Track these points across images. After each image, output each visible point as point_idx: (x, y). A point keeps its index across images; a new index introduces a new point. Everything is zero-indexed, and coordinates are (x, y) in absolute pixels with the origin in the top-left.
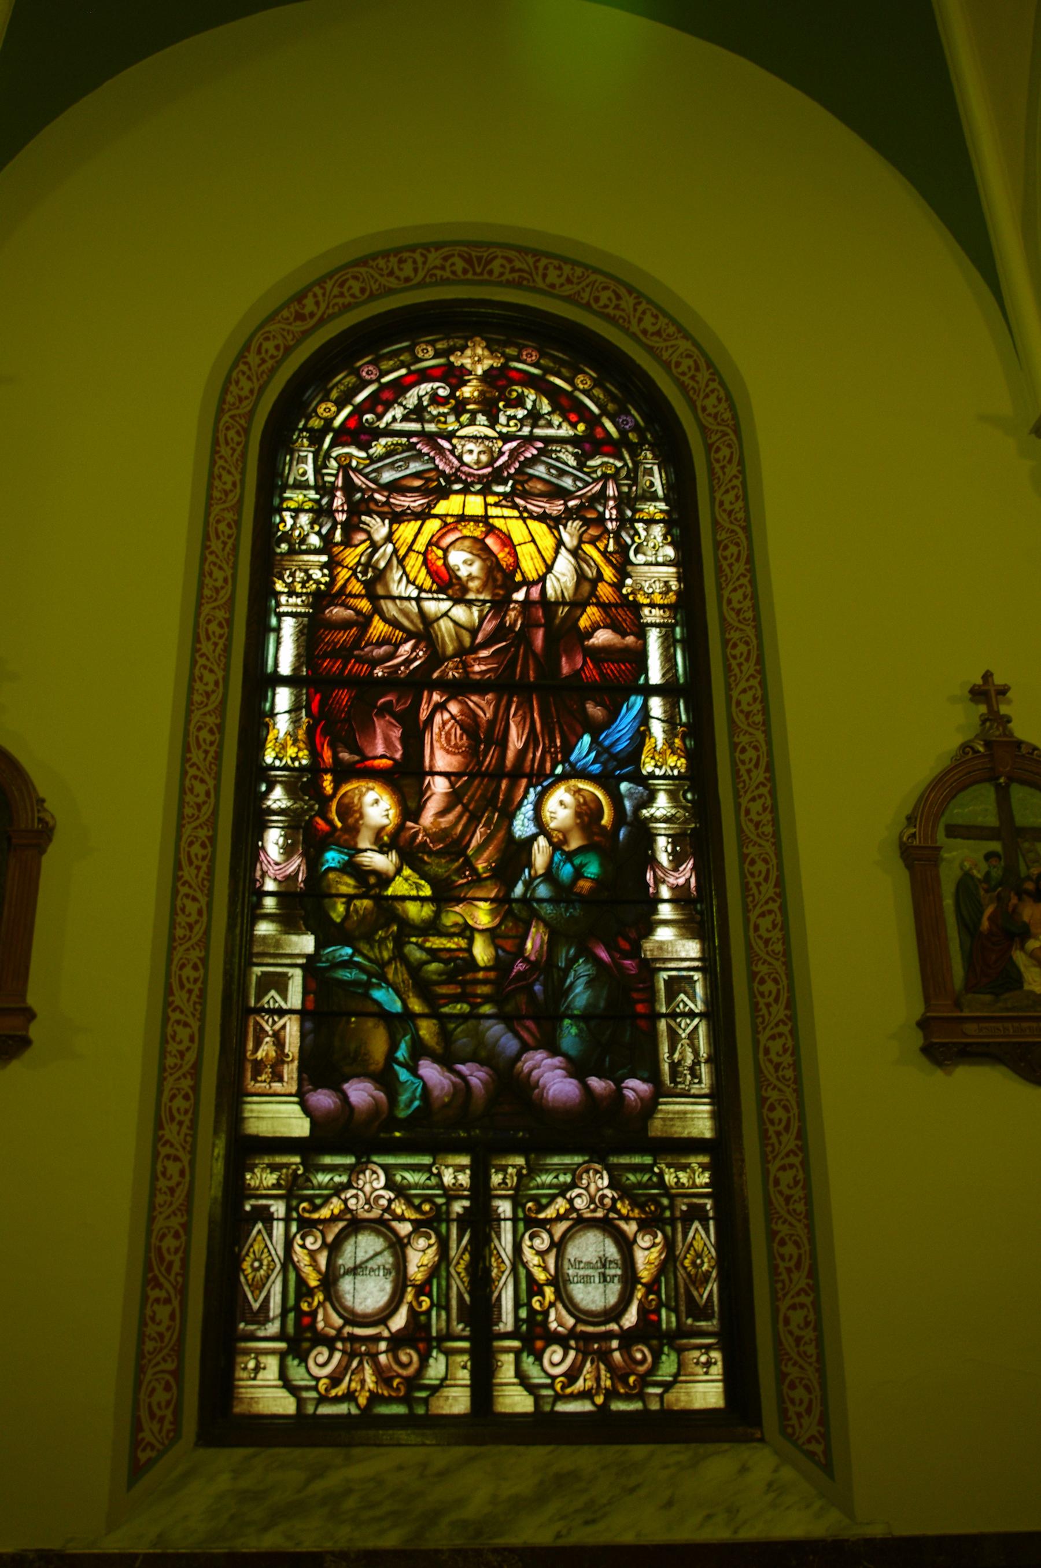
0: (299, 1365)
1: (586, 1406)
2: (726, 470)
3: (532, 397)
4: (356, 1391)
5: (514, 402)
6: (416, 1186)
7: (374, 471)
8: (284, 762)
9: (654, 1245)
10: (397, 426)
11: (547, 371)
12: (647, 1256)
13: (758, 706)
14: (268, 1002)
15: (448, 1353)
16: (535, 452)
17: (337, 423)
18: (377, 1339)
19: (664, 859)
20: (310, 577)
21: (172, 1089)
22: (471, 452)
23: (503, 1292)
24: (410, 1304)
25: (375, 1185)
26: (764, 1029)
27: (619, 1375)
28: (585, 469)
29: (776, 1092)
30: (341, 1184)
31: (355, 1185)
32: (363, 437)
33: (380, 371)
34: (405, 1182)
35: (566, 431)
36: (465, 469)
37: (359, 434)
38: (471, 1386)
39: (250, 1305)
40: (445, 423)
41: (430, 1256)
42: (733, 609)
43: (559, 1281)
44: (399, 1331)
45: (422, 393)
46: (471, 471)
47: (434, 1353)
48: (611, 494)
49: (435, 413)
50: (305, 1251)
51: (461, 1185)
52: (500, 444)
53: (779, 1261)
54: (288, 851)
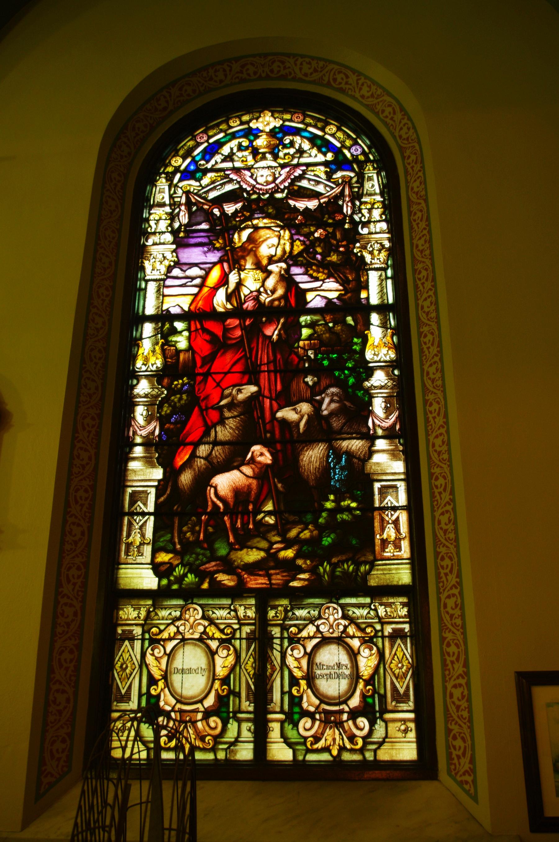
1: (325, 757)
2: (436, 420)
7: (205, 193)
9: (228, 655)
11: (308, 125)
12: (367, 662)
13: (433, 307)
14: (387, 503)
15: (239, 721)
16: (301, 172)
17: (182, 168)
18: (196, 711)
20: (165, 258)
22: (262, 176)
24: (217, 690)
26: (438, 508)
28: (332, 180)
29: (457, 727)
30: (176, 617)
35: (321, 158)
36: (257, 186)
41: (374, 661)
42: (430, 379)
43: (310, 678)
44: (356, 707)
47: (231, 721)
49: (240, 156)
50: (154, 658)
51: (249, 617)
52: (279, 169)
53: (452, 750)
54: (149, 419)
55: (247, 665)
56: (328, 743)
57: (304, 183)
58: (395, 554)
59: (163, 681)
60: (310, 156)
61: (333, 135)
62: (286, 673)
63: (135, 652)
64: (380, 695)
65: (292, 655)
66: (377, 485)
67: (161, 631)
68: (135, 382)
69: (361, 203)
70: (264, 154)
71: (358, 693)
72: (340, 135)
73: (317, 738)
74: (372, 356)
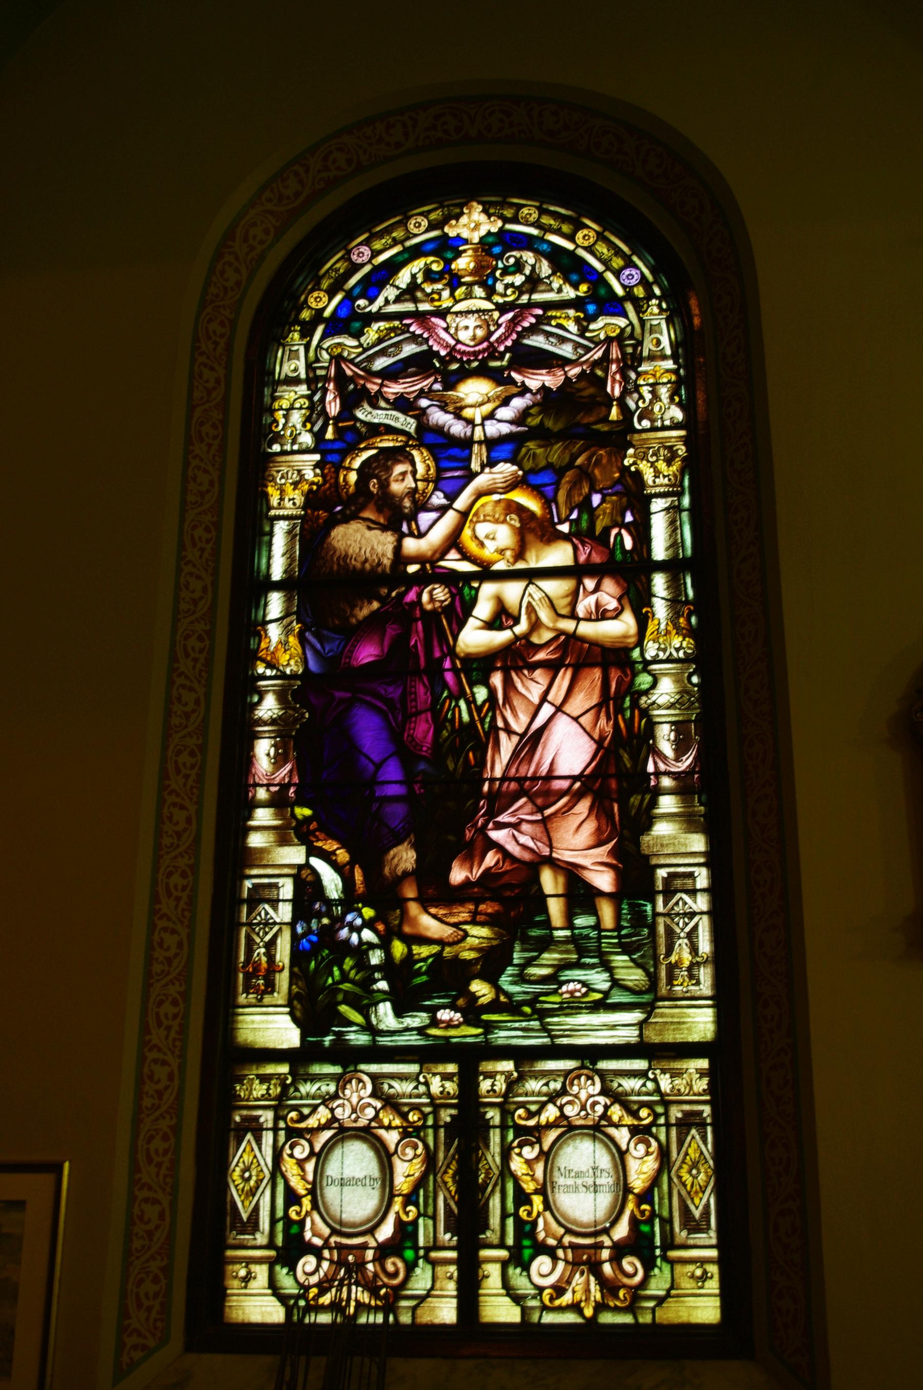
0: (287, 1274)
1: (570, 1318)
3: (532, 261)
4: (581, 1301)
5: (512, 269)
6: (633, 1092)
8: (667, 654)
10: (393, 308)
12: (642, 1168)
15: (434, 1263)
16: (533, 320)
17: (327, 313)
18: (364, 1247)
19: (667, 748)
20: (302, 476)
21: (159, 995)
22: (467, 328)
23: (261, 1201)
24: (397, 1213)
25: (362, 1093)
27: (609, 1287)
28: (588, 335)
30: (555, 1090)
31: (341, 1095)
32: (357, 325)
33: (372, 251)
34: (620, 1089)
35: (569, 293)
36: (459, 347)
37: (348, 322)
38: (457, 1297)
39: (240, 1215)
40: (439, 300)
41: (651, 1164)
45: (415, 271)
46: (468, 349)
47: (421, 1261)
48: (614, 356)
49: (429, 290)
50: (294, 1161)
51: (449, 1093)
52: (496, 315)
54: (278, 761)
55: (682, 1171)
56: (578, 1296)
57: (537, 341)
58: (691, 988)
59: (309, 1197)
60: (552, 290)
61: (590, 249)
62: (510, 1187)
63: (264, 1153)
64: (663, 1221)
65: (291, 1156)
66: (662, 873)
67: (303, 1118)
68: (256, 699)
69: (639, 375)
70: (470, 285)
71: (391, 1219)
72: (602, 248)
73: (559, 1290)
74: (653, 653)
